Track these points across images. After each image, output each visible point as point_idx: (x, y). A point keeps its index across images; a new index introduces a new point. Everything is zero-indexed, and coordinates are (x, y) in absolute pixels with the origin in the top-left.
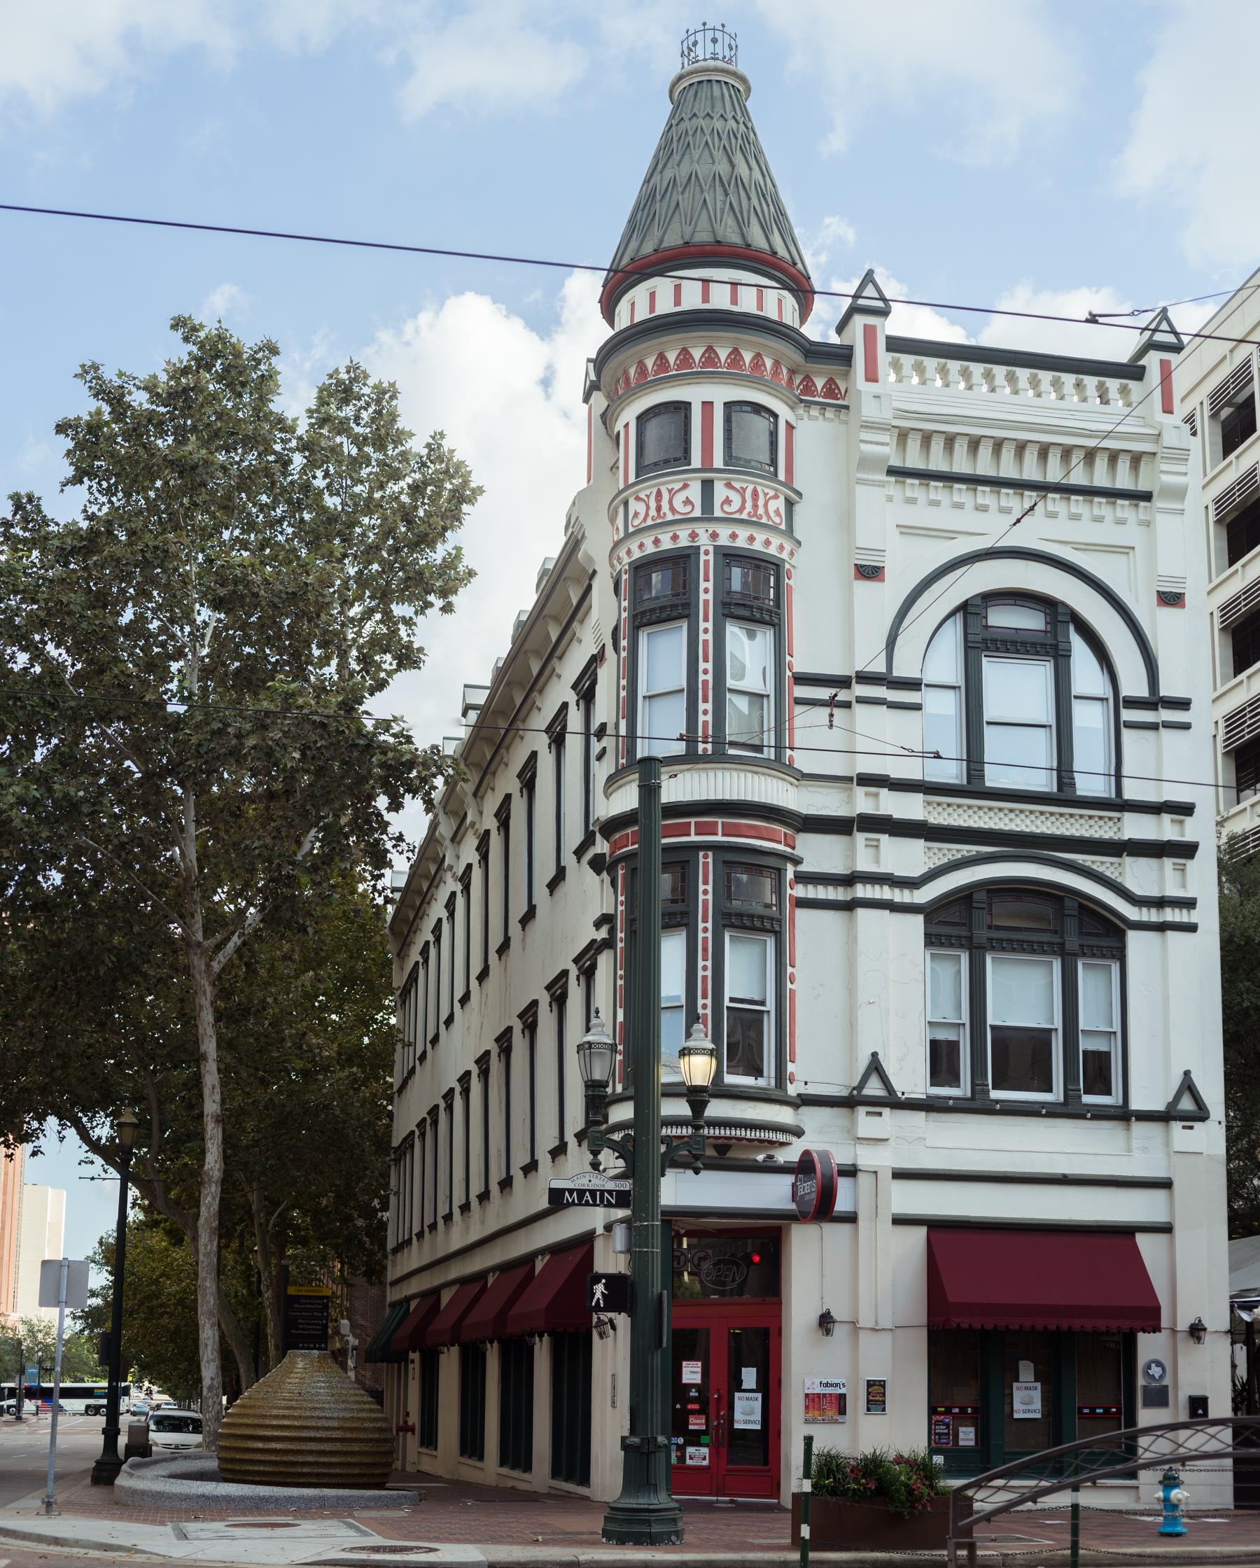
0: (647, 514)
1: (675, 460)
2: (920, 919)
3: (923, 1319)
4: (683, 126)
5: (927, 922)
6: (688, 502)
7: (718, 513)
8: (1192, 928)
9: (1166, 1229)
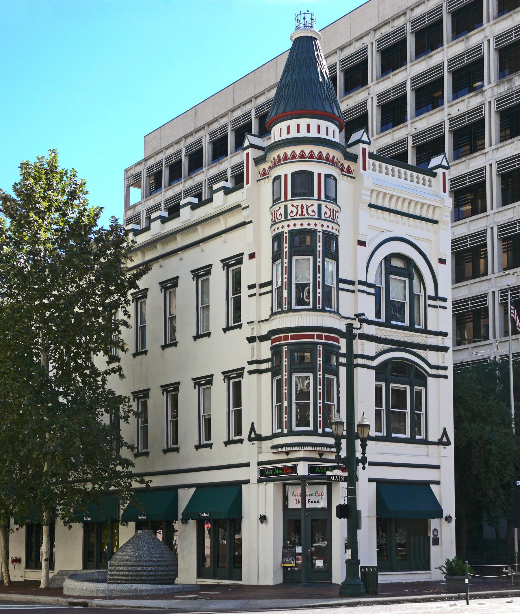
0: (297, 213)
2: (373, 372)
3: (375, 514)
5: (376, 373)
6: (313, 211)
7: (323, 217)
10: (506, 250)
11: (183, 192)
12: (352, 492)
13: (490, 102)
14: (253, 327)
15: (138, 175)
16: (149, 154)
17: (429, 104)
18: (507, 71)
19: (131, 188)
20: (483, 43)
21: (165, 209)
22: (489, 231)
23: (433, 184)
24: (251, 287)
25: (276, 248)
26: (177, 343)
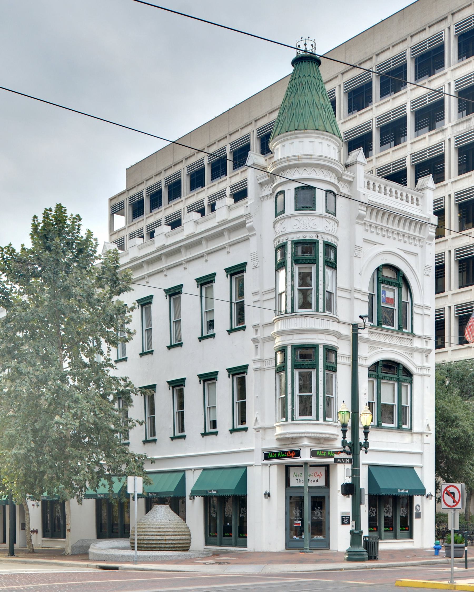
1: (310, 207)
4: (296, 81)
8: (429, 376)
9: (421, 467)
10: (461, 271)
11: (228, 188)
12: (355, 473)
13: (449, 140)
14: (256, 329)
15: (121, 204)
16: (131, 186)
17: (392, 141)
18: (465, 112)
19: (115, 215)
20: (444, 86)
21: (231, 195)
22: (447, 254)
23: (420, 203)
24: (255, 294)
25: (279, 258)
26: (182, 343)
